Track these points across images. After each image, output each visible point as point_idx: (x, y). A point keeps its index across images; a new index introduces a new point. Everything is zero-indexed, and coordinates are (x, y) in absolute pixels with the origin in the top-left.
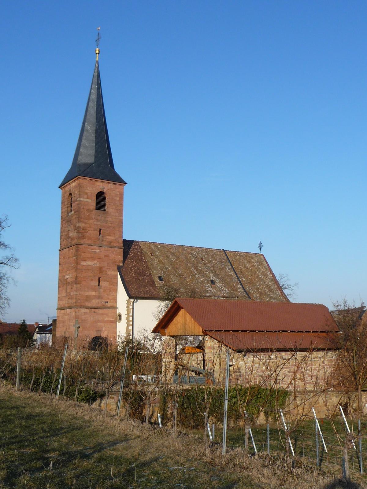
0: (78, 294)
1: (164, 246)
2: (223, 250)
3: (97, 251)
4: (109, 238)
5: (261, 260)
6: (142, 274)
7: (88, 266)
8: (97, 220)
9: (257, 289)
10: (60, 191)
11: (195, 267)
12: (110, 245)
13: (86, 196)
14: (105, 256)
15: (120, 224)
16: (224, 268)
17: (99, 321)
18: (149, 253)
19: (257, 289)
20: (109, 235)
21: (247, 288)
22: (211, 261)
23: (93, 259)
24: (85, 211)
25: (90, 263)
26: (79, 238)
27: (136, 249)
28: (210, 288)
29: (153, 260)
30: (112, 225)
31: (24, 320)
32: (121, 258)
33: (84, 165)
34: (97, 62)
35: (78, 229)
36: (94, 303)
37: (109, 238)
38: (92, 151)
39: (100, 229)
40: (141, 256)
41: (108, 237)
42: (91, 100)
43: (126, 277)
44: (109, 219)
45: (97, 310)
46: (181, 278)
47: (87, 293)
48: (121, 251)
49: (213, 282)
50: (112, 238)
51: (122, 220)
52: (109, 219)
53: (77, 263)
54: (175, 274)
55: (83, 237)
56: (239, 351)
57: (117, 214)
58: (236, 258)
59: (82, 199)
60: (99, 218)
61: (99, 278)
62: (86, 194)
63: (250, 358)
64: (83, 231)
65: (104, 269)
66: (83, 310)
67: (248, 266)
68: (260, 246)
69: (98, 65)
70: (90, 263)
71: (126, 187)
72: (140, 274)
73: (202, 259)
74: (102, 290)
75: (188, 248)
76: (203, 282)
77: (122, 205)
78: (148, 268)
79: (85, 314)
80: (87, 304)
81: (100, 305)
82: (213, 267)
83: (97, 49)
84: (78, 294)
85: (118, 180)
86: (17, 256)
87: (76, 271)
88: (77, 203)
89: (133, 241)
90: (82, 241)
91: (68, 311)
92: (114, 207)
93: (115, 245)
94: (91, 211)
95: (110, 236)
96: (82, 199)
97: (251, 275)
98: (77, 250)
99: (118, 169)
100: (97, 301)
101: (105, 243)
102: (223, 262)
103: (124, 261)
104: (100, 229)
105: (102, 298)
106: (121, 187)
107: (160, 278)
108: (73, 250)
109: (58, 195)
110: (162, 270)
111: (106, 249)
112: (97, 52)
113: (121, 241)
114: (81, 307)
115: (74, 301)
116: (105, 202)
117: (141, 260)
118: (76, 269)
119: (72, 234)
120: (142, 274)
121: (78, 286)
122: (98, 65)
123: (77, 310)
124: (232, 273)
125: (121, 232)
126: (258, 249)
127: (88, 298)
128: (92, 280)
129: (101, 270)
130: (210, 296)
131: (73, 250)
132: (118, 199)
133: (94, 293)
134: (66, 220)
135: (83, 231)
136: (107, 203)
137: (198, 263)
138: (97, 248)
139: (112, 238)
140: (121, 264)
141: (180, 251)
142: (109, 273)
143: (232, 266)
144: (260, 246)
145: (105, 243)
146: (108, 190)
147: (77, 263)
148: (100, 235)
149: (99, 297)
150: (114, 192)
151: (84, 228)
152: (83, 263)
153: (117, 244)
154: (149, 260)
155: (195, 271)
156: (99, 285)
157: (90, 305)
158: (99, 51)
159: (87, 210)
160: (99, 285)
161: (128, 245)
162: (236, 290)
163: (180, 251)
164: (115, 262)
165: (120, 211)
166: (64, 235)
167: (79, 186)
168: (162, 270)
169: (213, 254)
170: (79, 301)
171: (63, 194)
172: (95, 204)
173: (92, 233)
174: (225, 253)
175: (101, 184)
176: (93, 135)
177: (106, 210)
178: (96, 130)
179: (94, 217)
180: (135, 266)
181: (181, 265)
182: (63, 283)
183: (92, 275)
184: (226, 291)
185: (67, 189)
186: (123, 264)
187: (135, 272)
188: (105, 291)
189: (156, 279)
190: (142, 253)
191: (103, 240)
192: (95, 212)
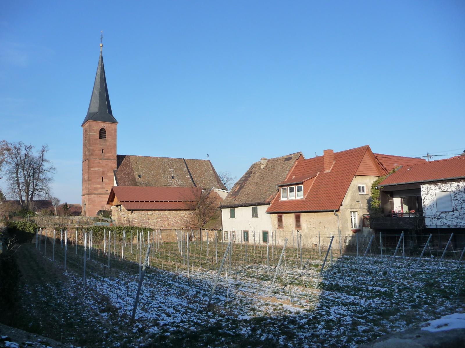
0: (89, 186)
1: (145, 158)
2: (183, 159)
3: (101, 162)
4: (108, 154)
5: (208, 164)
6: (129, 174)
7: (95, 170)
8: (101, 145)
9: (202, 181)
10: (82, 128)
11: (163, 170)
12: (108, 158)
13: (93, 131)
14: (106, 165)
15: (115, 146)
16: (182, 170)
17: (102, 201)
18: (135, 163)
19: (202, 181)
20: (108, 153)
21: (195, 181)
22: (174, 166)
23: (98, 167)
24: (93, 139)
25: (97, 169)
26: (89, 155)
27: (127, 160)
28: (171, 182)
29: (137, 166)
30: (109, 147)
31: (66, 203)
32: (115, 165)
33: (93, 113)
34: (101, 52)
35: (89, 150)
36: (100, 191)
37: (108, 154)
38: (97, 105)
39: (103, 150)
40: (129, 164)
41: (107, 154)
42: (97, 75)
43: (118, 176)
44: (108, 144)
45: (101, 195)
46: (153, 176)
47: (95, 186)
48: (116, 162)
49: (173, 178)
50: (110, 154)
51: (116, 144)
52: (108, 144)
53: (89, 169)
54: (149, 174)
55: (92, 155)
56: (129, 210)
57: (113, 141)
58: (191, 163)
59: (91, 133)
60: (102, 144)
61: (102, 177)
62: (94, 130)
63: (136, 213)
64: (92, 151)
65: (106, 172)
66: (93, 196)
67: (199, 168)
68: (208, 156)
69: (102, 54)
70: (97, 169)
71: (118, 125)
72: (127, 174)
73: (168, 165)
74: (104, 184)
75: (160, 159)
76: (167, 178)
77: (116, 135)
78: (132, 171)
79: (94, 197)
80: (95, 192)
81: (103, 193)
82: (175, 169)
83: (101, 44)
84: (89, 186)
85: (113, 121)
86: (55, 166)
87: (88, 174)
88: (88, 135)
89: (124, 156)
90: (92, 157)
91: (86, 196)
92: (111, 137)
93: (112, 158)
94: (97, 139)
95: (109, 153)
96: (91, 133)
97: (200, 173)
98: (89, 162)
99: (115, 114)
100: (101, 190)
101: (105, 158)
102: (182, 166)
103: (117, 168)
104: (103, 150)
105: (104, 189)
106: (115, 125)
107: (140, 176)
108: (87, 162)
109: (80, 131)
110: (142, 172)
111: (107, 160)
112: (101, 46)
113: (116, 156)
114: (91, 194)
115: (87, 191)
116: (105, 134)
117: (129, 166)
118: (88, 172)
119: (87, 153)
120: (129, 174)
121: (90, 182)
122: (102, 54)
123: (89, 195)
124: (187, 172)
125: (116, 151)
126: (207, 157)
127: (96, 189)
128: (98, 179)
129: (103, 173)
130: (169, 186)
131: (87, 162)
132: (113, 132)
133: (99, 186)
134: (85, 145)
135: (92, 151)
136: (107, 135)
137: (165, 167)
138: (101, 160)
139: (110, 154)
140: (116, 169)
141: (155, 160)
142: (108, 174)
143: (188, 168)
144: (208, 156)
145: (105, 158)
146: (106, 127)
147: (89, 169)
148: (102, 153)
149: (103, 188)
150: (111, 128)
151: (93, 150)
152: (92, 169)
153: (114, 158)
154: (134, 166)
155: (163, 172)
156: (102, 181)
157: (97, 193)
158: (102, 45)
159: (94, 139)
160: (102, 181)
161: (120, 159)
162: (188, 182)
163: (155, 160)
164: (112, 168)
165: (115, 139)
166: (84, 155)
167: (89, 126)
168: (142, 172)
169: (176, 162)
170: (90, 191)
171: (84, 130)
172: (99, 136)
173: (98, 152)
174: (184, 160)
175: (102, 124)
176: (98, 96)
177: (106, 139)
178: (100, 93)
179: (98, 143)
180: (124, 170)
181: (154, 169)
182: (84, 181)
183: (98, 175)
184: (180, 183)
185: (85, 127)
186: (117, 169)
187: (124, 173)
188: (106, 184)
189: (137, 177)
190: (130, 162)
191: (104, 156)
192: (99, 140)
